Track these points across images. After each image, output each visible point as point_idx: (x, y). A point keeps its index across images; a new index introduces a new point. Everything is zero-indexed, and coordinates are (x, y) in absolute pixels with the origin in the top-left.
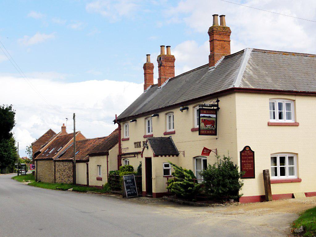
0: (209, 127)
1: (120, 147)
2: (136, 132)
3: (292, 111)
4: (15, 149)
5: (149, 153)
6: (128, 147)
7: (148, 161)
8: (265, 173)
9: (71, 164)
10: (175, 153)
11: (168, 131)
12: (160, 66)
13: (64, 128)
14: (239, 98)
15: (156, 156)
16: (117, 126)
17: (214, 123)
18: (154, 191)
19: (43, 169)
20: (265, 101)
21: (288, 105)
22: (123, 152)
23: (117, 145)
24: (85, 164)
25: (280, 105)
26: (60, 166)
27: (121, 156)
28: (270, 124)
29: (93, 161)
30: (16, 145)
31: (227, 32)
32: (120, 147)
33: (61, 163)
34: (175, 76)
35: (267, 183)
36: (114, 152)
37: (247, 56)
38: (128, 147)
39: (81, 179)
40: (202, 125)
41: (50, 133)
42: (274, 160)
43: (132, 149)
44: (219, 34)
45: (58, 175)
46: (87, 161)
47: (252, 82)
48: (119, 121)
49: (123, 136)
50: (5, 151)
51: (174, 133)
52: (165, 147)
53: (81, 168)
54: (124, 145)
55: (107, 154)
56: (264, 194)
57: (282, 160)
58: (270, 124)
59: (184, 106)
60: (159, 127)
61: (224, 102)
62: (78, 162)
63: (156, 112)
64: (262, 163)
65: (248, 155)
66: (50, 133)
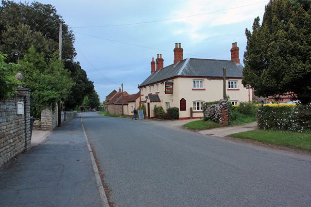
0: (169, 91)
1: (140, 99)
2: (146, 92)
3: (237, 85)
4: (98, 99)
5: (149, 101)
6: (143, 98)
7: (149, 104)
8: (191, 109)
9: (121, 106)
10: (159, 101)
11: (157, 92)
12: (157, 63)
13: (120, 89)
14: (179, 79)
15: (151, 102)
16: (139, 90)
17: (172, 89)
18: (150, 116)
19: (110, 108)
20: (191, 80)
21: (235, 83)
22: (142, 100)
23: (139, 98)
24: (127, 106)
25: (232, 83)
26: (117, 107)
27: (141, 102)
28: (193, 90)
29: (130, 104)
30: (99, 98)
31: (162, 60)
32: (140, 99)
33: (117, 106)
34: (164, 67)
35: (192, 112)
36: (138, 101)
37: (187, 62)
38: (143, 98)
39: (126, 113)
40: (166, 90)
41: (115, 91)
42: (194, 103)
43: (145, 99)
44: (178, 51)
45: (116, 111)
46: (127, 105)
47: (186, 73)
48: (140, 87)
49: (142, 94)
50: (94, 101)
51: (159, 93)
52: (155, 98)
53: (125, 107)
54: (142, 97)
55: (135, 101)
56: (102, 92)
57: (198, 104)
58: (193, 90)
59: (162, 82)
60: (153, 90)
61: (175, 81)
62: (124, 105)
63: (153, 84)
64: (189, 105)
65: (183, 102)
66: (115, 91)
